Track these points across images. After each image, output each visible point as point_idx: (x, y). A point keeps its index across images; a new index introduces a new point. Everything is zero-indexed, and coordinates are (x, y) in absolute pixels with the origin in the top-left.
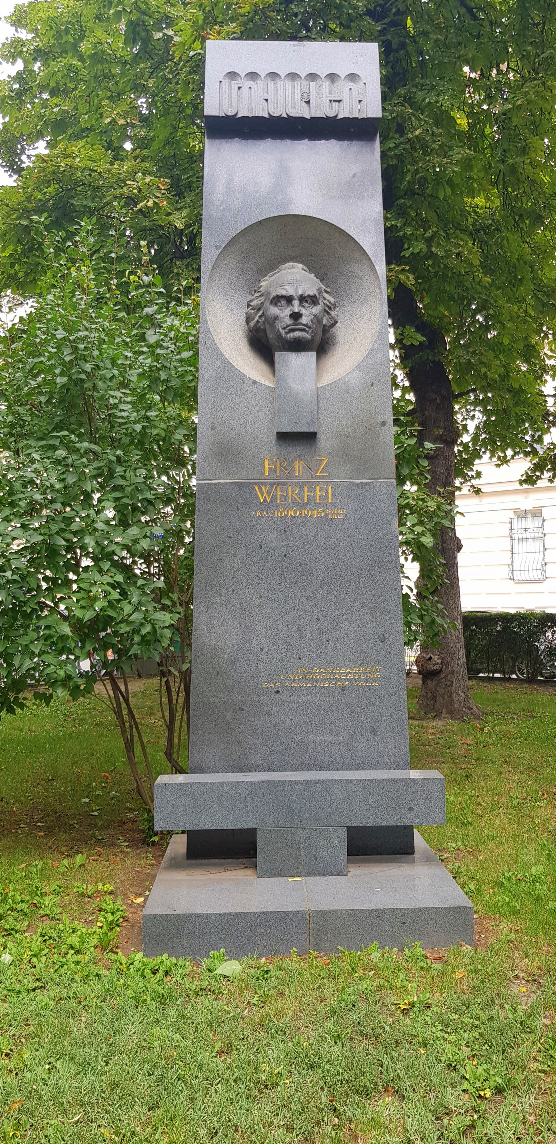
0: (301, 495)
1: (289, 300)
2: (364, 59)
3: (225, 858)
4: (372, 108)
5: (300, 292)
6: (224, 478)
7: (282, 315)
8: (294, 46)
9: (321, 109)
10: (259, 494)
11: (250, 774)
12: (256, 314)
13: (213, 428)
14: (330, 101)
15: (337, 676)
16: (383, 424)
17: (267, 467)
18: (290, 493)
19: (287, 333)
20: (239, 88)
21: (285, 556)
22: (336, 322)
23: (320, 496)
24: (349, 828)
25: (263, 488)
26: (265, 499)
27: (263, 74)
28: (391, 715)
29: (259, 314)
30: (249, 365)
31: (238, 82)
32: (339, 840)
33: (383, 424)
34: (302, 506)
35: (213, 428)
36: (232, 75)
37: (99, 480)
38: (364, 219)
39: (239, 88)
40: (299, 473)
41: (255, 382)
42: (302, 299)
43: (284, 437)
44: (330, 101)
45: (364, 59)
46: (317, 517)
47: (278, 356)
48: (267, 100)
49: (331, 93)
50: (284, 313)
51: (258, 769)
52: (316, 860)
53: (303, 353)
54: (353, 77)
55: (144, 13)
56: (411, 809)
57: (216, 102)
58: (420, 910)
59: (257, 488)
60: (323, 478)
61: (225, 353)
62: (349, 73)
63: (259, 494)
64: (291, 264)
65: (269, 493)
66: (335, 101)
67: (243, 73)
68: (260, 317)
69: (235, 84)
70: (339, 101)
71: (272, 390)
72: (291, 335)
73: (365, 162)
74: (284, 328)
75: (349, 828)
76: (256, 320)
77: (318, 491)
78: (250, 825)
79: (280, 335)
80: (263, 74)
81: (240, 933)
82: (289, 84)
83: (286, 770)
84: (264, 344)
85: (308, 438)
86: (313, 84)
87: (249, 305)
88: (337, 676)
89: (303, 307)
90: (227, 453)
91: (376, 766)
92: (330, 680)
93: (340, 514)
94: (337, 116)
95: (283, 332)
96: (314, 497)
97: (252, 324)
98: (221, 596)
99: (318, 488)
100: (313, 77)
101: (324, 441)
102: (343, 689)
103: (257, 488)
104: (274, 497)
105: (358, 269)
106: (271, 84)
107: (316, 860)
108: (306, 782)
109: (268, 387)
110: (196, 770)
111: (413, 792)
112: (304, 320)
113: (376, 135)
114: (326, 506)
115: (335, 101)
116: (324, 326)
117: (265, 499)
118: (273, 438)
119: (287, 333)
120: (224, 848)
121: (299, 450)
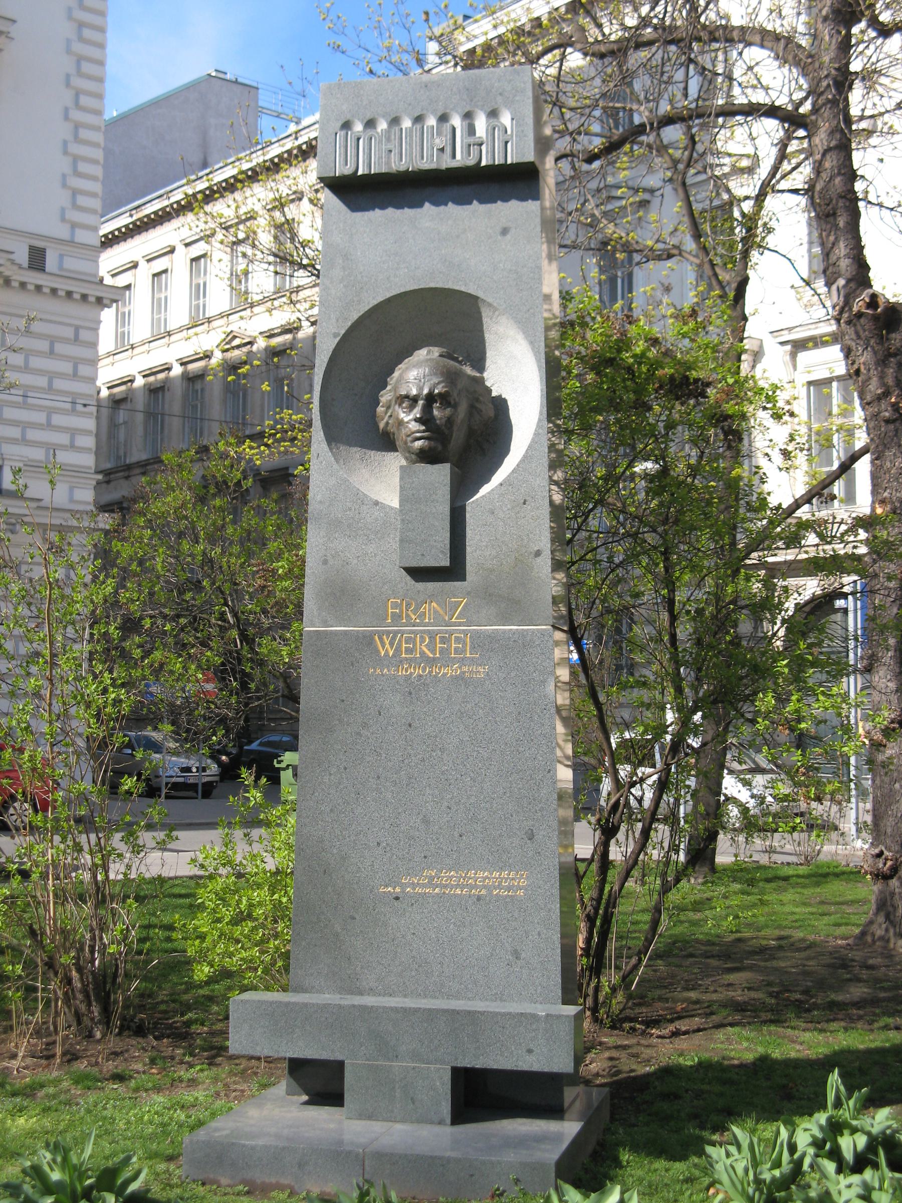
13: (325, 562)
34: (432, 662)
35: (325, 562)
51: (371, 991)
65: (391, 644)
90: (344, 595)
102: (479, 898)
104: (398, 650)
114: (462, 661)
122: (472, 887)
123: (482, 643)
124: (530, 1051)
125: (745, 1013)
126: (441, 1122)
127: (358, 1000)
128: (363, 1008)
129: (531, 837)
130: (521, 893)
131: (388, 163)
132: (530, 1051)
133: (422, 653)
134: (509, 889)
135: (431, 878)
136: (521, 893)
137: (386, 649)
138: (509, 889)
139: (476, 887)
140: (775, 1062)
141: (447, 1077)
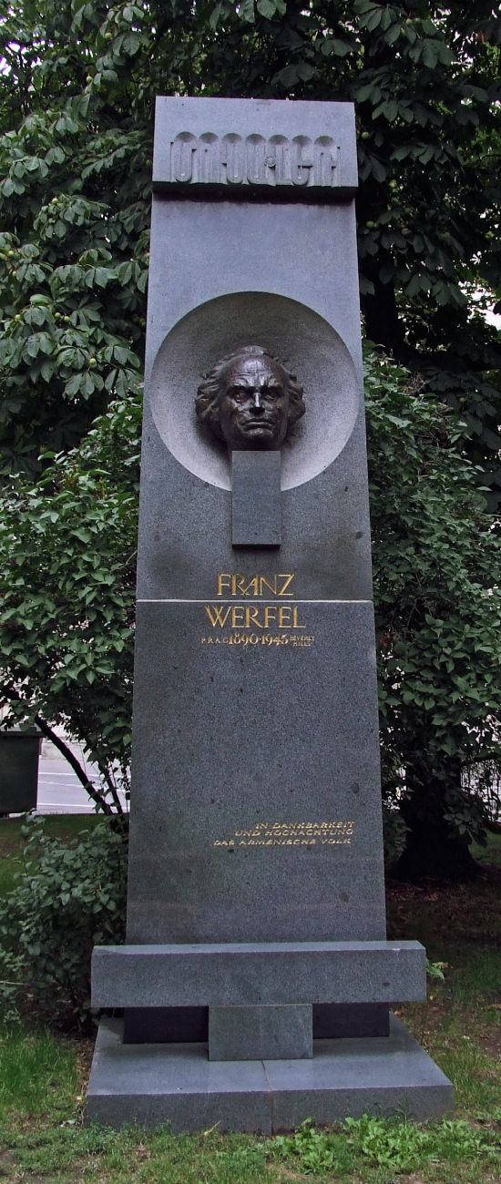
0: (261, 618)
2: (338, 119)
3: (161, 1098)
7: (240, 409)
8: (258, 104)
10: (211, 617)
11: (198, 945)
12: (208, 404)
13: (157, 539)
14: (299, 167)
15: (301, 833)
16: (359, 535)
18: (248, 616)
20: (193, 150)
21: (242, 691)
22: (303, 412)
23: (284, 619)
24: (316, 1008)
25: (216, 610)
27: (221, 135)
28: (365, 878)
29: (212, 404)
30: (204, 467)
31: (192, 144)
32: (305, 1019)
33: (359, 535)
34: (262, 632)
35: (157, 539)
36: (185, 136)
39: (193, 150)
40: (259, 592)
41: (207, 485)
43: (239, 549)
44: (299, 167)
45: (338, 119)
46: (280, 645)
47: (235, 455)
48: (225, 165)
51: (208, 940)
52: (277, 1041)
54: (324, 141)
56: (386, 984)
57: (166, 166)
58: (395, 1090)
59: (208, 610)
60: (288, 598)
61: (171, 451)
62: (318, 137)
63: (211, 617)
65: (222, 616)
66: (304, 167)
67: (195, 130)
68: (213, 407)
69: (188, 146)
70: (309, 167)
71: (229, 495)
73: (341, 229)
74: (243, 424)
76: (208, 410)
77: (281, 613)
78: (203, 1003)
79: (239, 431)
80: (221, 135)
81: (189, 1115)
83: (240, 942)
84: (218, 434)
86: (279, 148)
87: (199, 393)
88: (301, 833)
89: (266, 399)
92: (293, 838)
93: (307, 641)
94: (307, 183)
96: (277, 622)
97: (204, 414)
98: (165, 737)
99: (281, 610)
101: (290, 555)
102: (309, 847)
103: (208, 610)
106: (230, 146)
107: (277, 1041)
109: (222, 490)
110: (138, 941)
111: (390, 965)
112: (267, 414)
113: (351, 200)
115: (304, 167)
118: (227, 553)
121: (262, 561)
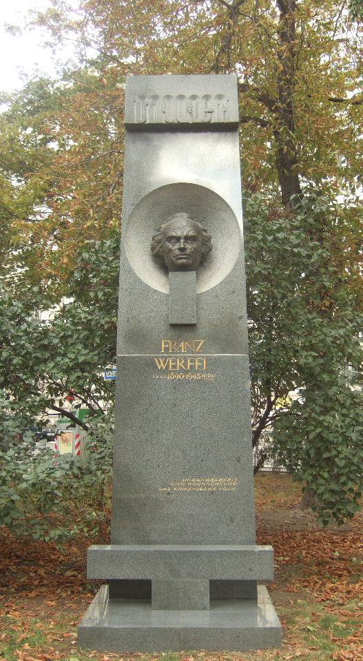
1: (178, 239)
4: (234, 117)
5: (185, 234)
6: (219, 353)
9: (201, 118)
13: (128, 321)
17: (163, 346)
19: (176, 260)
26: (162, 368)
30: (155, 281)
32: (204, 587)
33: (241, 318)
34: (186, 372)
35: (128, 321)
37: (28, 108)
38: (229, 188)
42: (187, 238)
49: (206, 107)
50: (175, 247)
51: (155, 543)
53: (189, 272)
54: (220, 97)
55: (58, 335)
64: (180, 214)
65: (164, 363)
68: (160, 247)
70: (211, 112)
72: (179, 261)
74: (174, 257)
75: (212, 583)
76: (158, 249)
79: (173, 261)
82: (179, 102)
84: (164, 262)
85: (191, 327)
90: (138, 338)
91: (234, 542)
93: (211, 376)
95: (174, 259)
97: (155, 252)
100: (194, 97)
101: (203, 330)
102: (212, 492)
104: (168, 366)
105: (224, 215)
108: (184, 552)
110: (116, 543)
114: (202, 372)
116: (202, 253)
117: (162, 368)
119: (176, 260)
120: (131, 592)
122: (208, 487)
123: (213, 364)
124: (251, 570)
125: (241, 543)
126: (205, 609)
127: (152, 548)
128: (162, 553)
129: (239, 460)
130: (234, 489)
131: (144, 116)
132: (251, 570)
133: (181, 368)
134: (227, 487)
135: (186, 483)
136: (234, 489)
137: (161, 365)
138: (227, 487)
139: (210, 487)
140: (224, 581)
141: (207, 585)
